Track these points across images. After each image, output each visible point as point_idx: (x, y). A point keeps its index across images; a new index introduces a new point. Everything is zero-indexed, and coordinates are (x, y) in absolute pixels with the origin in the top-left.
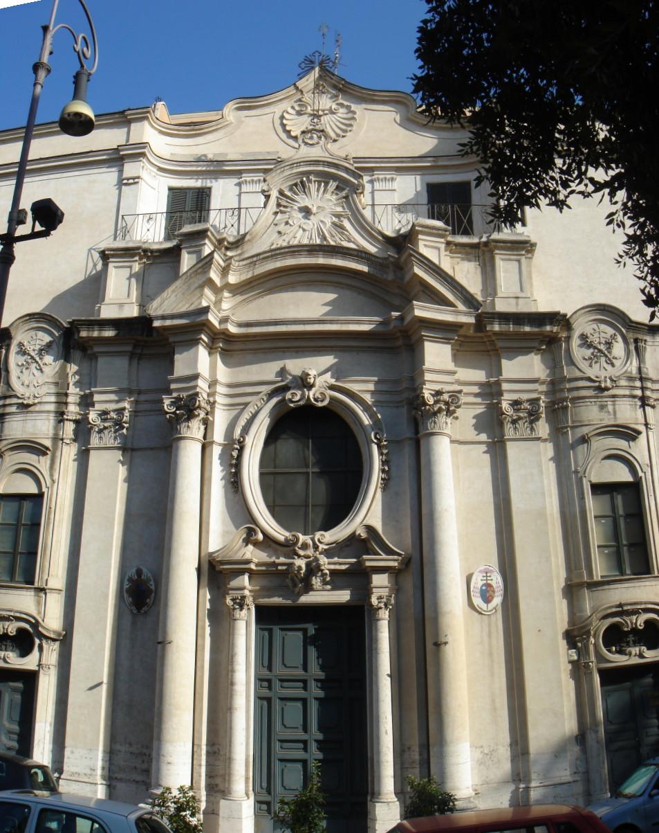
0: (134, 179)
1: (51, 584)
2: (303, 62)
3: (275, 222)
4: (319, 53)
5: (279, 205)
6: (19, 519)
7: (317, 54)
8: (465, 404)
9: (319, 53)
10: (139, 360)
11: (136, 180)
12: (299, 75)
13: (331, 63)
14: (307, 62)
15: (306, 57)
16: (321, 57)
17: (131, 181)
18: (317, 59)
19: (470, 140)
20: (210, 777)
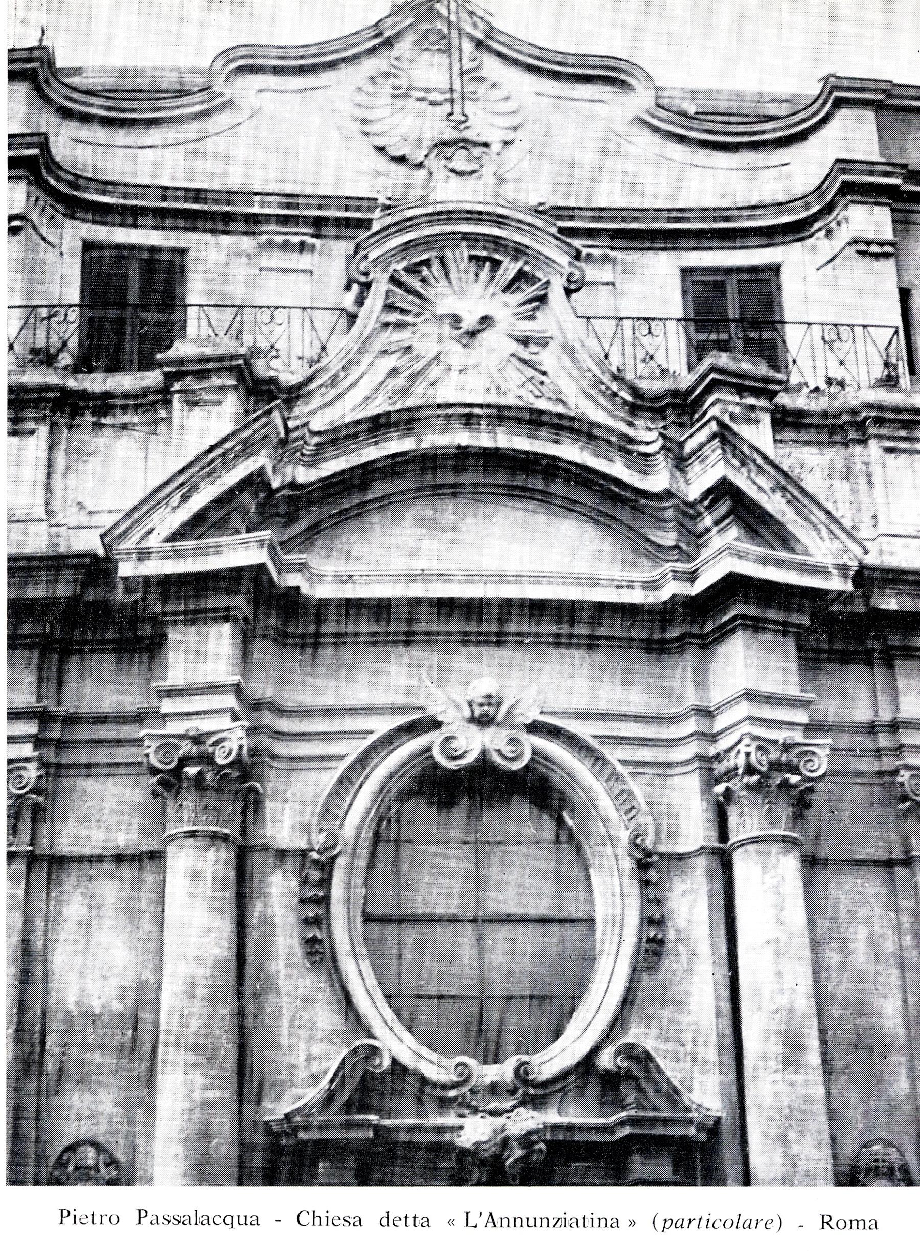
5: (390, 307)
17: (874, 249)
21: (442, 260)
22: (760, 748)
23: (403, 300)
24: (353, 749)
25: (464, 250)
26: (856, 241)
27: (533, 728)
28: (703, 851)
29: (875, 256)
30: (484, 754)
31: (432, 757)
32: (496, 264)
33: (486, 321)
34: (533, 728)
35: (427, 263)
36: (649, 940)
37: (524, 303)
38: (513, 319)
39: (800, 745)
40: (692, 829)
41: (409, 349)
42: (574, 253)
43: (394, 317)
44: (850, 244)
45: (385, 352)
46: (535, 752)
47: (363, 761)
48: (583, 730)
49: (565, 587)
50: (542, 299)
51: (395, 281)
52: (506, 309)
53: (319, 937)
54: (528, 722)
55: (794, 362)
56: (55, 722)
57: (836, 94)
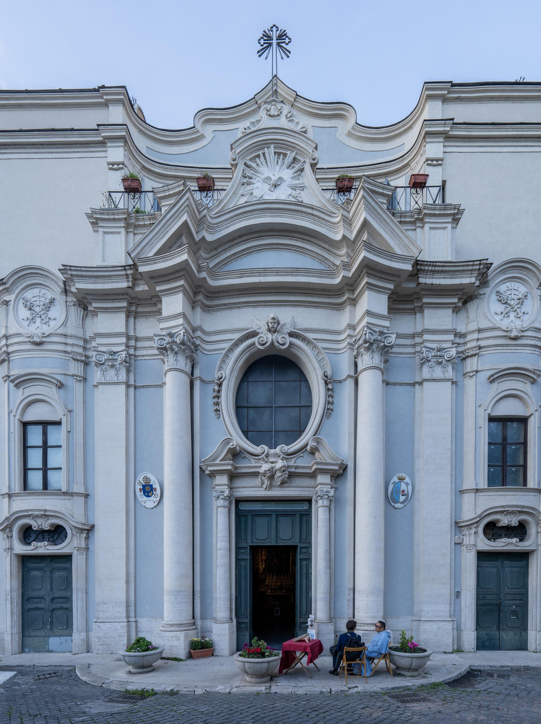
0: (437, 161)
1: (68, 297)
2: (262, 38)
3: (478, 404)
4: (277, 27)
6: (82, 361)
7: (274, 29)
8: (134, 333)
9: (277, 27)
10: (135, 318)
11: (440, 162)
12: (258, 52)
13: (287, 39)
14: (265, 38)
15: (264, 31)
16: (278, 32)
17: (435, 162)
18: (275, 35)
19: (252, 181)
20: (67, 609)
21: (264, 154)
22: (370, 333)
23: (249, 173)
24: (227, 345)
25: (272, 149)
26: (427, 160)
27: (291, 335)
28: (349, 376)
29: (435, 165)
30: (272, 343)
31: (256, 346)
32: (285, 155)
33: (280, 179)
34: (291, 335)
35: (258, 156)
36: (328, 409)
37: (296, 172)
38: (290, 180)
39: (386, 333)
40: (346, 369)
41: (252, 194)
42: (314, 146)
43: (245, 180)
44: (425, 162)
45: (243, 195)
46: (291, 344)
47: (231, 350)
48: (311, 336)
49: (447, 526)
50: (302, 170)
51: (245, 164)
52: (287, 174)
53: (218, 408)
54: (289, 332)
55: (398, 204)
56: (132, 339)
57: (427, 93)
